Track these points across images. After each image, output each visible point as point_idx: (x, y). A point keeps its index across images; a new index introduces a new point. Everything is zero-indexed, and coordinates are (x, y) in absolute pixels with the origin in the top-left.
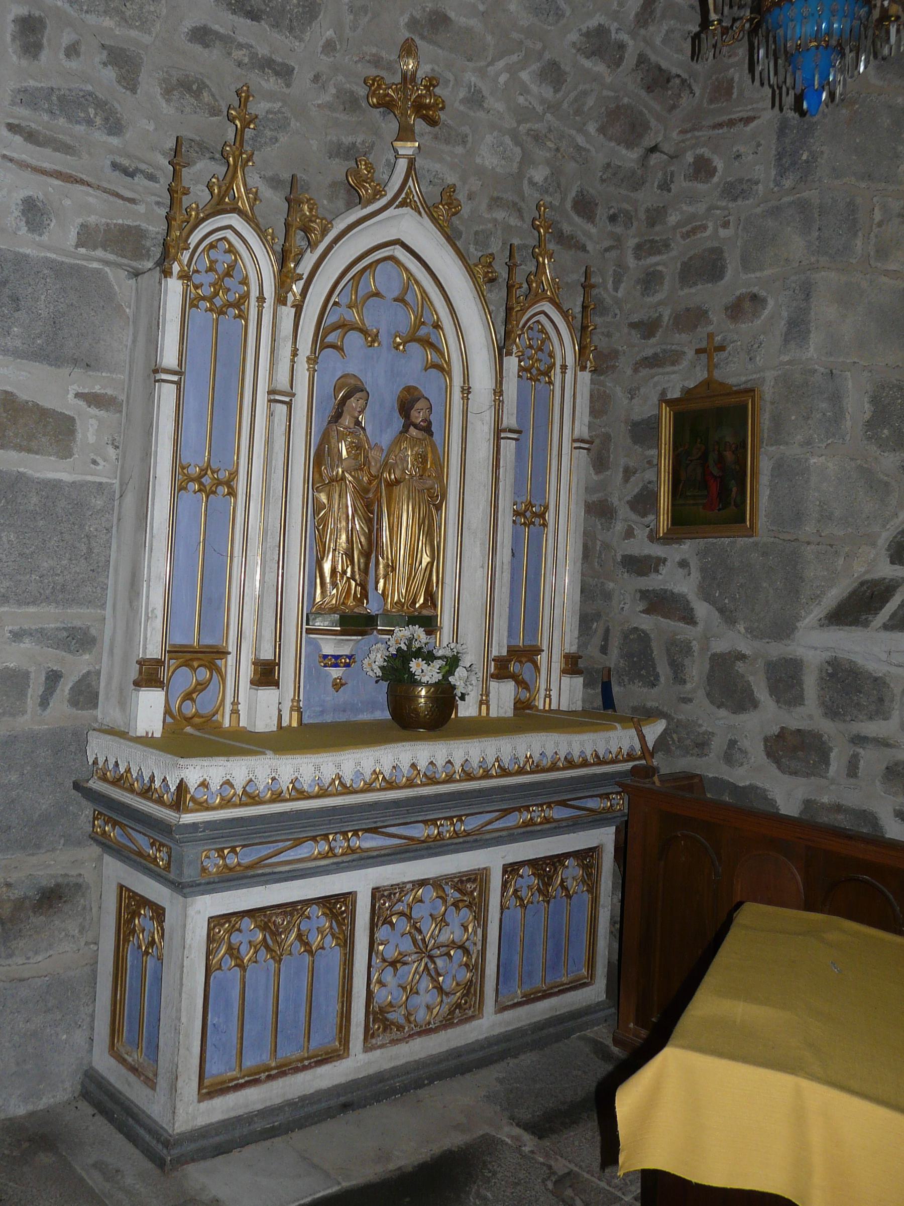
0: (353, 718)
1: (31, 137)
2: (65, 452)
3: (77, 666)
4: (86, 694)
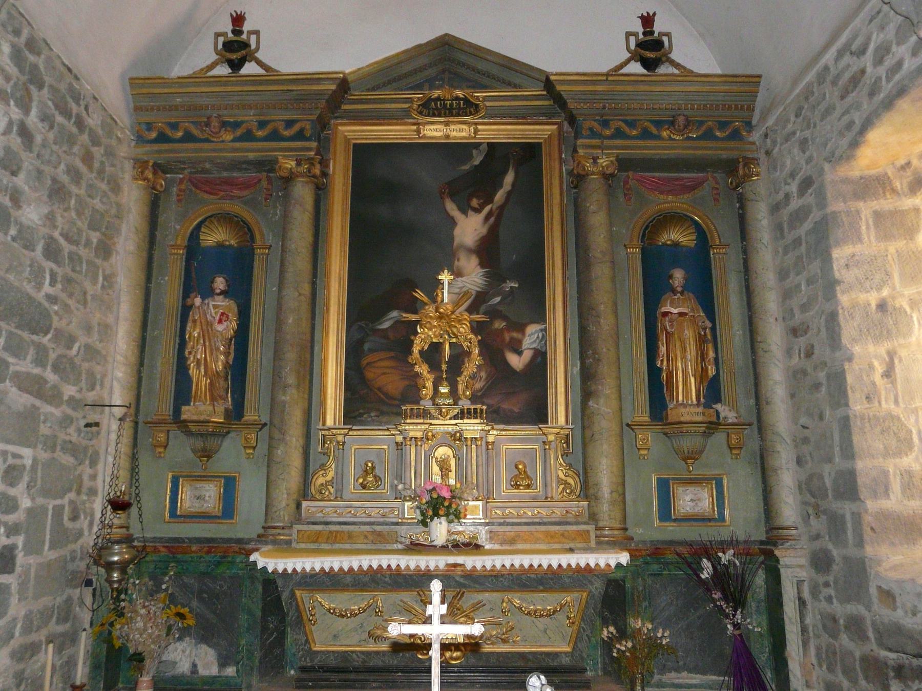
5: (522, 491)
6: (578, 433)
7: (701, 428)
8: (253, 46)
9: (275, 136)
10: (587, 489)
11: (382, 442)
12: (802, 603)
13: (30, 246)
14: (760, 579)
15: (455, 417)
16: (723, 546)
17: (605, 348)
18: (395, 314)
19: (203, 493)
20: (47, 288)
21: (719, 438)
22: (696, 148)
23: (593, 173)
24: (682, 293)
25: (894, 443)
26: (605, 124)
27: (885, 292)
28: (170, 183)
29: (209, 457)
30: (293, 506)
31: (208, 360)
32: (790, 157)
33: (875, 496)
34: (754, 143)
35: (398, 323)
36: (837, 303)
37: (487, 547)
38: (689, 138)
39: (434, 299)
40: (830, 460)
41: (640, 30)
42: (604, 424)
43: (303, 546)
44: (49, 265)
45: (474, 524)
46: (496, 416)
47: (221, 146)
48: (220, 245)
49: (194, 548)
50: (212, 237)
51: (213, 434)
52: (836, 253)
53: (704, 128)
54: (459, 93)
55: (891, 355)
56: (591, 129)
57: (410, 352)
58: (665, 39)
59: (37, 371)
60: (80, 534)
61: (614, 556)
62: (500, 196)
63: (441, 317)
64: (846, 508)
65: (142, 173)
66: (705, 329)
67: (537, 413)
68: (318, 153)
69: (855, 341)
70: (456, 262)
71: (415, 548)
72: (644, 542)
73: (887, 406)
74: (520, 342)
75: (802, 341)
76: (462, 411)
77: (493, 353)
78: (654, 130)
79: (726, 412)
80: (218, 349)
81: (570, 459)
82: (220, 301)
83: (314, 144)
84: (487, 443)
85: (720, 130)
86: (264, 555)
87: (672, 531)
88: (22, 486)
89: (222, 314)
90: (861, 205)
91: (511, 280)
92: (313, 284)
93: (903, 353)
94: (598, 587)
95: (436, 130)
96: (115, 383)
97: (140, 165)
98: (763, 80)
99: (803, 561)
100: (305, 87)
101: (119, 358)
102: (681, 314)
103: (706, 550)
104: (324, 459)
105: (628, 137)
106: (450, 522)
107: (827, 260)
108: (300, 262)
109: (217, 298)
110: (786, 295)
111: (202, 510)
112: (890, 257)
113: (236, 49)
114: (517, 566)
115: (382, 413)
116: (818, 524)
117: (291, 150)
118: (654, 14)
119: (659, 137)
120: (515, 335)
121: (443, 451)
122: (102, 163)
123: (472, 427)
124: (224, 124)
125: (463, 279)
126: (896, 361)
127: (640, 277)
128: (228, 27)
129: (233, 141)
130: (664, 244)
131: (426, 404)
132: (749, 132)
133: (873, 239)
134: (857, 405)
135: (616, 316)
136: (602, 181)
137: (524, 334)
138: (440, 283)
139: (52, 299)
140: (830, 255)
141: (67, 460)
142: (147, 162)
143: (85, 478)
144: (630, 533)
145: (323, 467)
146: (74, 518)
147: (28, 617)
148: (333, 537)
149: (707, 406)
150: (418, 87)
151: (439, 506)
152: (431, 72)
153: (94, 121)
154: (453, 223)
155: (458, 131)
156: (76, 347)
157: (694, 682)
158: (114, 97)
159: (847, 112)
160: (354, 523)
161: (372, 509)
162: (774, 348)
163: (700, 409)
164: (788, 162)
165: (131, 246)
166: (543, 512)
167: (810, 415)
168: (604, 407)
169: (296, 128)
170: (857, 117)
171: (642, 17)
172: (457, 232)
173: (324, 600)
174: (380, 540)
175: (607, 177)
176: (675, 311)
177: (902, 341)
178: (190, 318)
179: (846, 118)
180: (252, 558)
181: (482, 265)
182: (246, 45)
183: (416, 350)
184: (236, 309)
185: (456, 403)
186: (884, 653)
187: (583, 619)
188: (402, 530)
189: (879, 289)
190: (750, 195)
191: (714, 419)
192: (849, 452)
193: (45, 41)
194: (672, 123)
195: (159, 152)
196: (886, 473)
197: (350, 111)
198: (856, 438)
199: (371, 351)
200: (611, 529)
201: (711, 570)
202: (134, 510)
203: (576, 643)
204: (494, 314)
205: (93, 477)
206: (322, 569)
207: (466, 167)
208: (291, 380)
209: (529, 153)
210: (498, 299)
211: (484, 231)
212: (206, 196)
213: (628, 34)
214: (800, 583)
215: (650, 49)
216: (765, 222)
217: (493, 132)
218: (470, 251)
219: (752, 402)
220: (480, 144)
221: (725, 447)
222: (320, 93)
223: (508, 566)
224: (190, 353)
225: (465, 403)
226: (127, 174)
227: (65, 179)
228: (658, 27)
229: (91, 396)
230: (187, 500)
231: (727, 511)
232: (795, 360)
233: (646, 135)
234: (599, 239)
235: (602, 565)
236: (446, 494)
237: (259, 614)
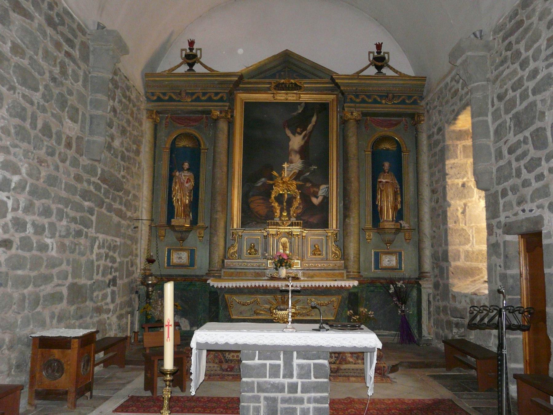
5: (317, 256)
6: (341, 233)
7: (393, 231)
8: (199, 56)
9: (210, 100)
10: (344, 256)
11: (258, 235)
12: (429, 302)
13: (116, 157)
14: (414, 293)
15: (289, 226)
16: (399, 280)
17: (353, 196)
18: (263, 179)
19: (181, 256)
20: (122, 173)
21: (401, 235)
22: (397, 108)
23: (351, 119)
24: (388, 173)
25: (463, 240)
26: (357, 96)
27: (465, 180)
28: (161, 119)
29: (183, 241)
30: (221, 262)
31: (182, 198)
32: (435, 117)
33: (454, 260)
34: (422, 106)
35: (264, 184)
36: (446, 182)
37: (302, 279)
38: (394, 104)
39: (280, 175)
40: (441, 246)
41: (375, 50)
42: (352, 229)
43: (226, 278)
44: (122, 163)
45: (296, 270)
46: (307, 225)
47: (186, 104)
48: (184, 147)
49: (178, 279)
50: (183, 143)
51: (186, 231)
52: (447, 162)
53: (401, 99)
54: (293, 81)
55: (465, 205)
56: (351, 99)
57: (270, 197)
58: (386, 56)
59: (120, 207)
60: (133, 272)
61: (351, 282)
62: (310, 127)
63: (284, 183)
64: (444, 264)
65: (151, 115)
66: (397, 189)
67: (324, 224)
68: (230, 108)
69: (452, 199)
70: (290, 157)
71: (272, 278)
72: (367, 278)
73: (462, 225)
74: (317, 193)
75: (435, 196)
76: (292, 223)
77: (306, 199)
78: (379, 100)
79: (404, 224)
80: (186, 194)
81: (337, 243)
82: (186, 173)
83: (228, 104)
84: (303, 236)
85: (408, 100)
86: (212, 280)
87: (380, 274)
88: (117, 253)
89: (188, 179)
90: (458, 142)
91: (314, 166)
92: (228, 166)
93: (469, 204)
94: (345, 294)
95: (282, 96)
96: (143, 210)
97: (150, 112)
98: (427, 78)
99: (431, 286)
100: (225, 79)
101: (145, 199)
102: (387, 182)
103: (392, 281)
104: (232, 242)
105: (367, 103)
106: (287, 268)
107: (444, 165)
108: (222, 157)
109: (185, 172)
110: (432, 175)
111: (181, 263)
112: (468, 165)
113: (191, 58)
114: (313, 286)
115: (258, 223)
116: (437, 271)
117: (217, 106)
118: (382, 43)
119: (380, 103)
120: (315, 189)
121: (284, 240)
122: (136, 115)
123: (296, 230)
124: (187, 94)
125: (293, 164)
126: (467, 208)
127: (370, 163)
128: (187, 47)
129: (192, 101)
130: (383, 149)
131: (277, 220)
132: (421, 101)
133: (462, 157)
134: (451, 225)
135: (359, 182)
136: (355, 123)
137: (319, 189)
138: (284, 168)
139: (123, 177)
140: (445, 162)
141: (129, 242)
142: (153, 111)
143: (134, 250)
144: (361, 274)
145: (232, 245)
146: (132, 266)
147: (121, 304)
148: (238, 274)
149: (397, 221)
150: (273, 76)
151: (282, 262)
152: (279, 68)
153: (133, 97)
154: (289, 139)
155: (291, 97)
156: (131, 195)
157: (385, 334)
158: (137, 82)
159: (453, 105)
160: (247, 269)
161: (251, 263)
162: (425, 197)
163: (393, 223)
164: (434, 118)
165: (147, 149)
166: (325, 265)
167: (436, 227)
168: (353, 221)
169: (219, 96)
170: (456, 108)
171: (376, 44)
172: (291, 143)
173: (236, 298)
174: (258, 275)
175: (358, 121)
176: (384, 181)
177: (469, 199)
178: (174, 180)
179: (452, 108)
180: (208, 282)
181: (301, 158)
182: (195, 56)
183: (273, 196)
184: (193, 177)
185: (289, 220)
186: (452, 319)
187: (339, 307)
188: (267, 272)
189: (463, 178)
190: (420, 130)
191: (399, 227)
192: (447, 244)
193: (119, 69)
194: (387, 96)
195: (158, 106)
196: (459, 251)
197: (242, 87)
198: (449, 238)
199: (253, 196)
200: (354, 272)
201: (393, 289)
202: (156, 263)
203: (336, 316)
204: (306, 180)
205: (136, 249)
206: (236, 286)
207: (295, 114)
208: (219, 209)
209: (324, 107)
210: (308, 174)
211: (302, 143)
212: (178, 125)
213: (370, 53)
214: (429, 295)
215: (380, 61)
216: (425, 142)
217: (306, 98)
218: (296, 152)
219: (416, 220)
220: (302, 103)
221: (404, 240)
222: (231, 81)
223: (310, 286)
224: (174, 196)
225: (293, 220)
226: (144, 116)
227: (125, 125)
228: (383, 50)
229: (135, 215)
230: (175, 259)
231: (403, 266)
232: (433, 204)
233: (375, 102)
234: (353, 149)
235: (347, 286)
236: (285, 257)
237: (207, 305)
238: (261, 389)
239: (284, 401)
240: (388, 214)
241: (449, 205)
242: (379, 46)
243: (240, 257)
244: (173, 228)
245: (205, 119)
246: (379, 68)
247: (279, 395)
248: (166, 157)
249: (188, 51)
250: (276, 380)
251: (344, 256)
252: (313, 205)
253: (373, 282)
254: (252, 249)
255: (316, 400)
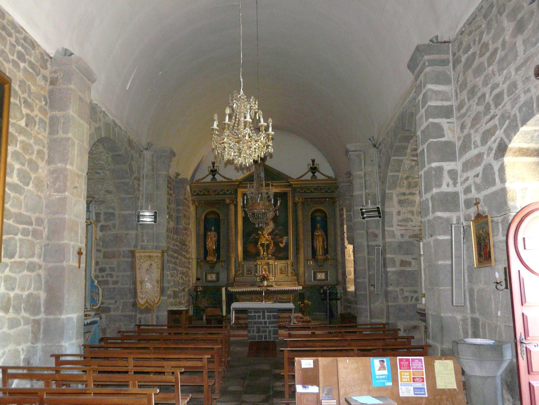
0: (179, 309)
1: (401, 226)
2: (410, 267)
3: (415, 295)
4: (417, 299)
9: (225, 194)
31: (211, 245)
46: (278, 258)
57: (257, 244)
58: (317, 166)
77: (276, 244)
79: (328, 256)
87: (316, 283)
103: (322, 287)
113: (214, 172)
119: (314, 193)
121: (265, 267)
131: (261, 256)
151: (264, 278)
161: (249, 279)
169: (229, 192)
174: (252, 285)
182: (216, 170)
183: (259, 244)
194: (317, 189)
215: (314, 169)
230: (209, 278)
233: (312, 192)
234: (300, 218)
238: (255, 323)
239: (262, 327)
240: (320, 252)
241: (346, 248)
242: (313, 161)
243: (243, 276)
244: (208, 262)
245: (221, 203)
246: (313, 173)
247: (261, 325)
248: (202, 224)
249: (212, 168)
250: (260, 320)
251: (297, 275)
252: (281, 248)
253: (312, 287)
254: (249, 271)
255: (273, 327)
